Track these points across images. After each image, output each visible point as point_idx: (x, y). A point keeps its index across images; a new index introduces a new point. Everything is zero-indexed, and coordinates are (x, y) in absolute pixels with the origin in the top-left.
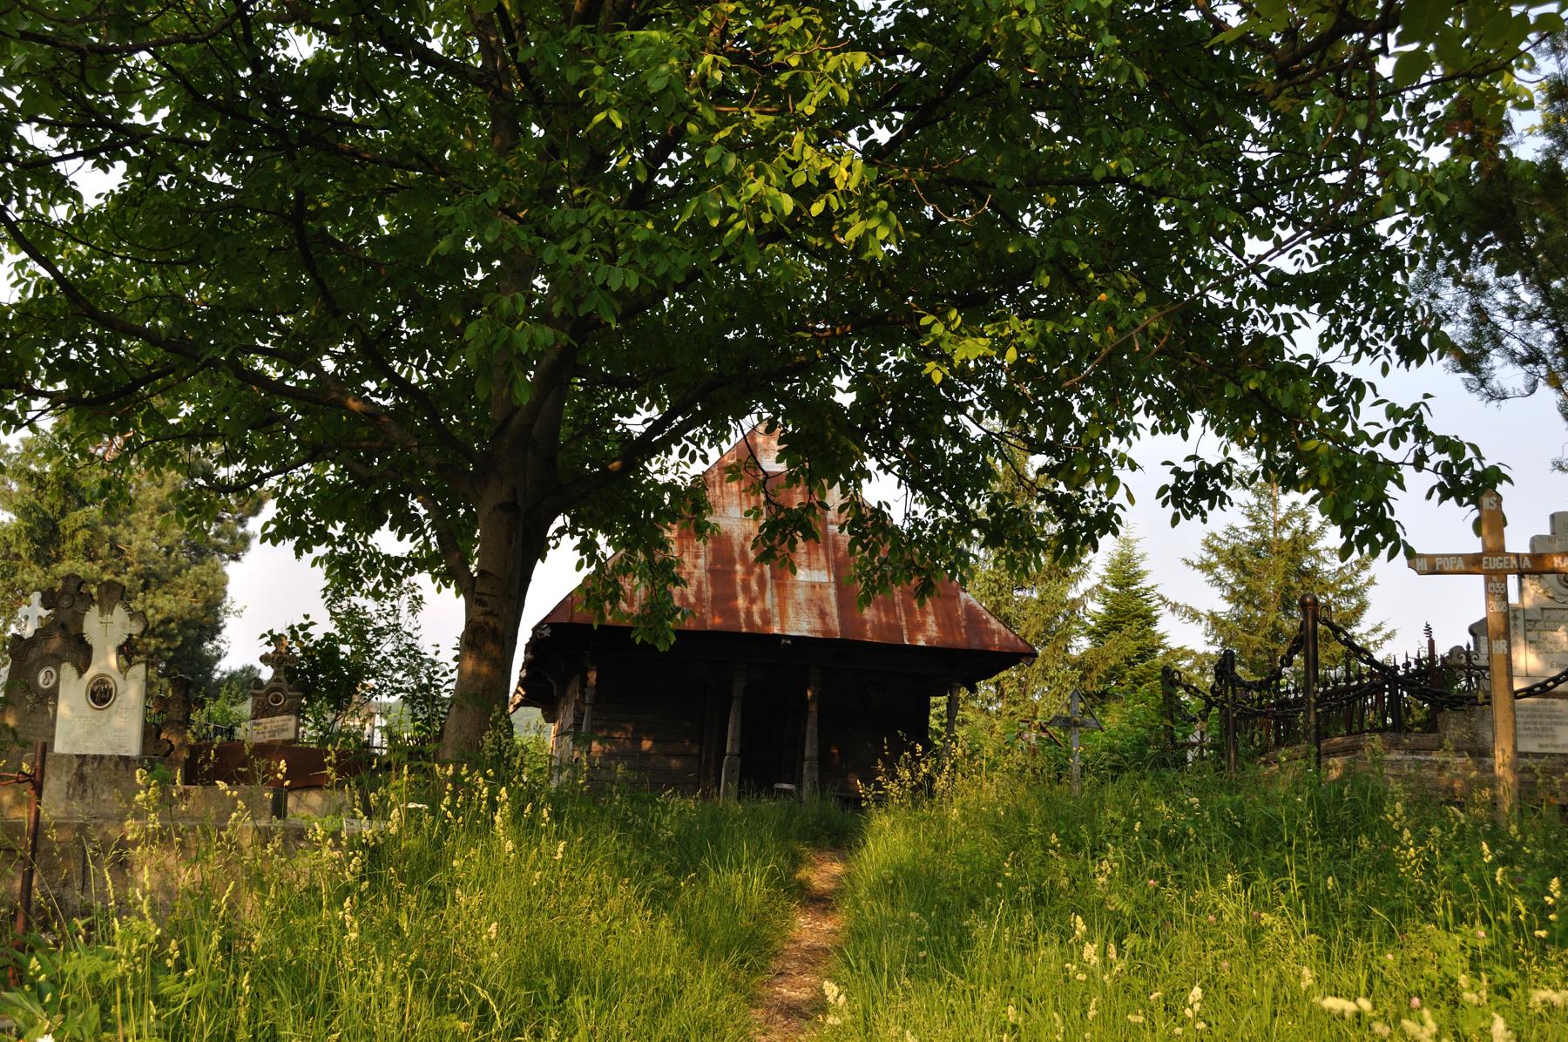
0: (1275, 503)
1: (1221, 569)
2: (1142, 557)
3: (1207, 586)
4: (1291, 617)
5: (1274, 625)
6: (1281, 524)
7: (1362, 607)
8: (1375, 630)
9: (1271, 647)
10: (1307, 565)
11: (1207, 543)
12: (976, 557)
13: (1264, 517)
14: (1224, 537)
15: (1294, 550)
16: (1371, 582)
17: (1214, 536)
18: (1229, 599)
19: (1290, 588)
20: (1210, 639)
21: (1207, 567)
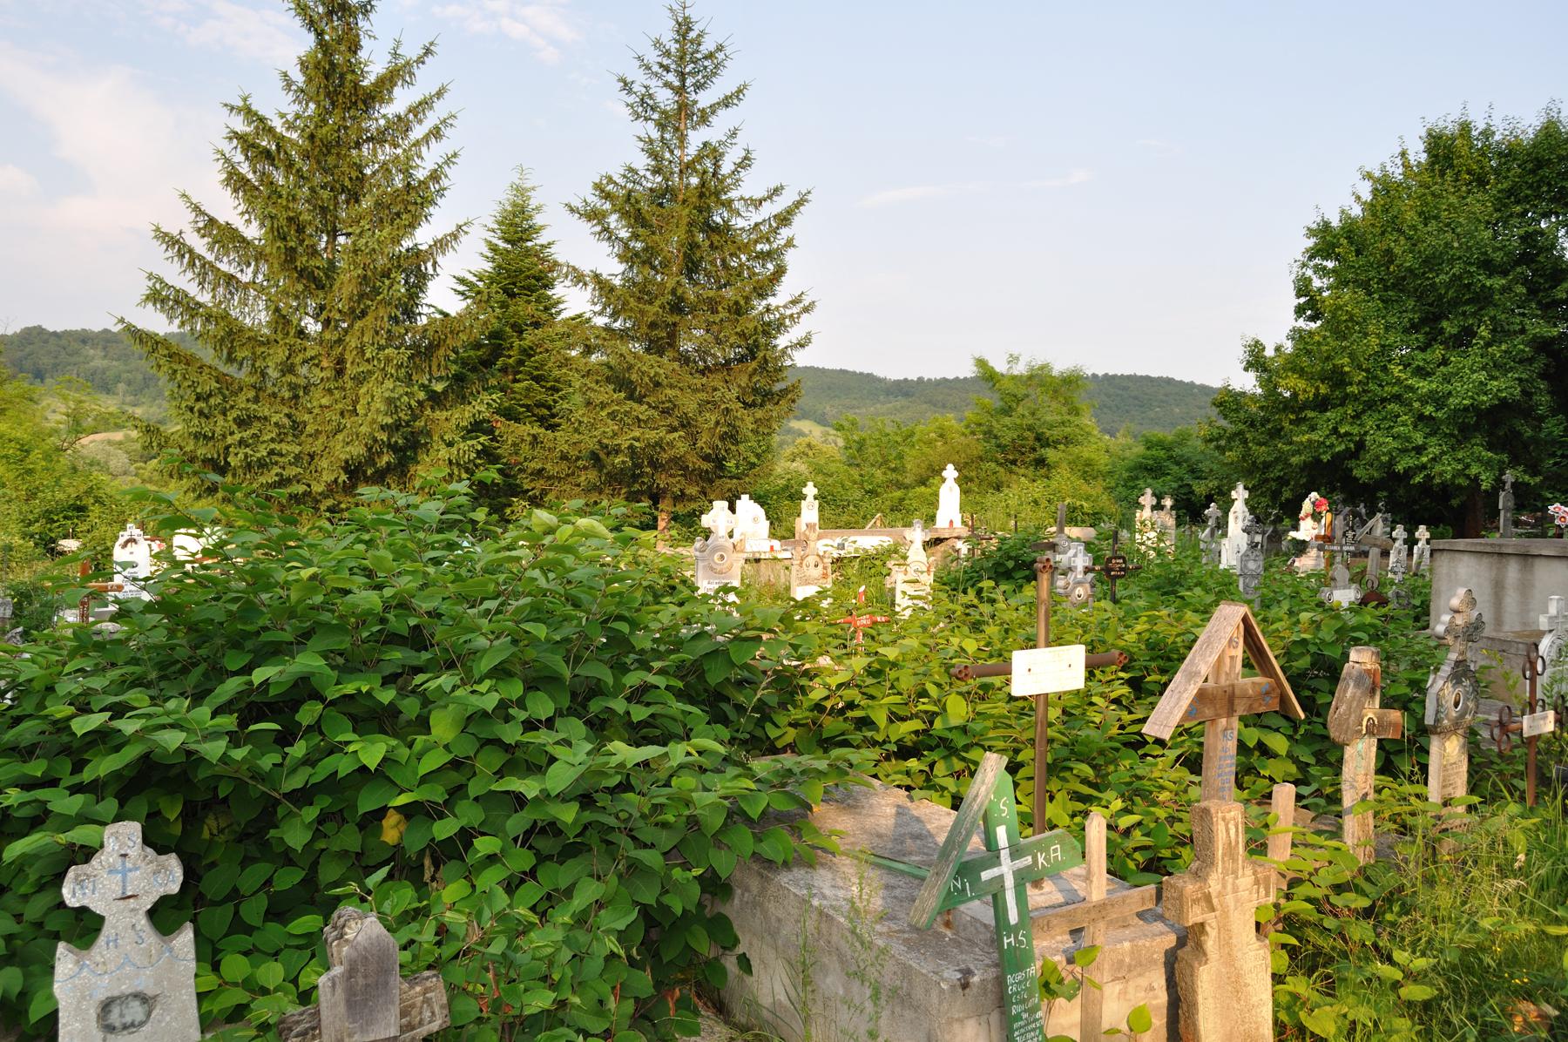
0: (683, 139)
1: (613, 220)
2: (538, 209)
3: (593, 240)
4: (696, 284)
5: (673, 292)
6: (688, 168)
7: (780, 271)
8: (794, 302)
9: (670, 320)
10: (718, 219)
11: (598, 187)
12: (1496, 379)
13: (667, 155)
14: (621, 181)
15: (702, 195)
16: (790, 243)
17: (610, 180)
18: (622, 258)
19: (694, 246)
20: (598, 308)
21: (593, 215)
